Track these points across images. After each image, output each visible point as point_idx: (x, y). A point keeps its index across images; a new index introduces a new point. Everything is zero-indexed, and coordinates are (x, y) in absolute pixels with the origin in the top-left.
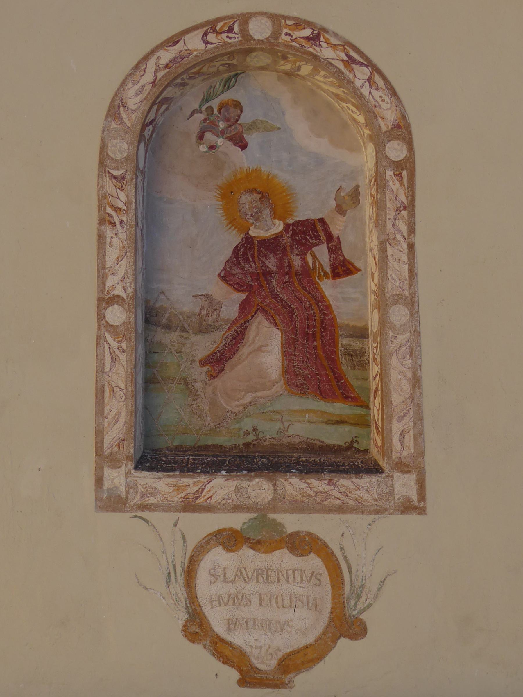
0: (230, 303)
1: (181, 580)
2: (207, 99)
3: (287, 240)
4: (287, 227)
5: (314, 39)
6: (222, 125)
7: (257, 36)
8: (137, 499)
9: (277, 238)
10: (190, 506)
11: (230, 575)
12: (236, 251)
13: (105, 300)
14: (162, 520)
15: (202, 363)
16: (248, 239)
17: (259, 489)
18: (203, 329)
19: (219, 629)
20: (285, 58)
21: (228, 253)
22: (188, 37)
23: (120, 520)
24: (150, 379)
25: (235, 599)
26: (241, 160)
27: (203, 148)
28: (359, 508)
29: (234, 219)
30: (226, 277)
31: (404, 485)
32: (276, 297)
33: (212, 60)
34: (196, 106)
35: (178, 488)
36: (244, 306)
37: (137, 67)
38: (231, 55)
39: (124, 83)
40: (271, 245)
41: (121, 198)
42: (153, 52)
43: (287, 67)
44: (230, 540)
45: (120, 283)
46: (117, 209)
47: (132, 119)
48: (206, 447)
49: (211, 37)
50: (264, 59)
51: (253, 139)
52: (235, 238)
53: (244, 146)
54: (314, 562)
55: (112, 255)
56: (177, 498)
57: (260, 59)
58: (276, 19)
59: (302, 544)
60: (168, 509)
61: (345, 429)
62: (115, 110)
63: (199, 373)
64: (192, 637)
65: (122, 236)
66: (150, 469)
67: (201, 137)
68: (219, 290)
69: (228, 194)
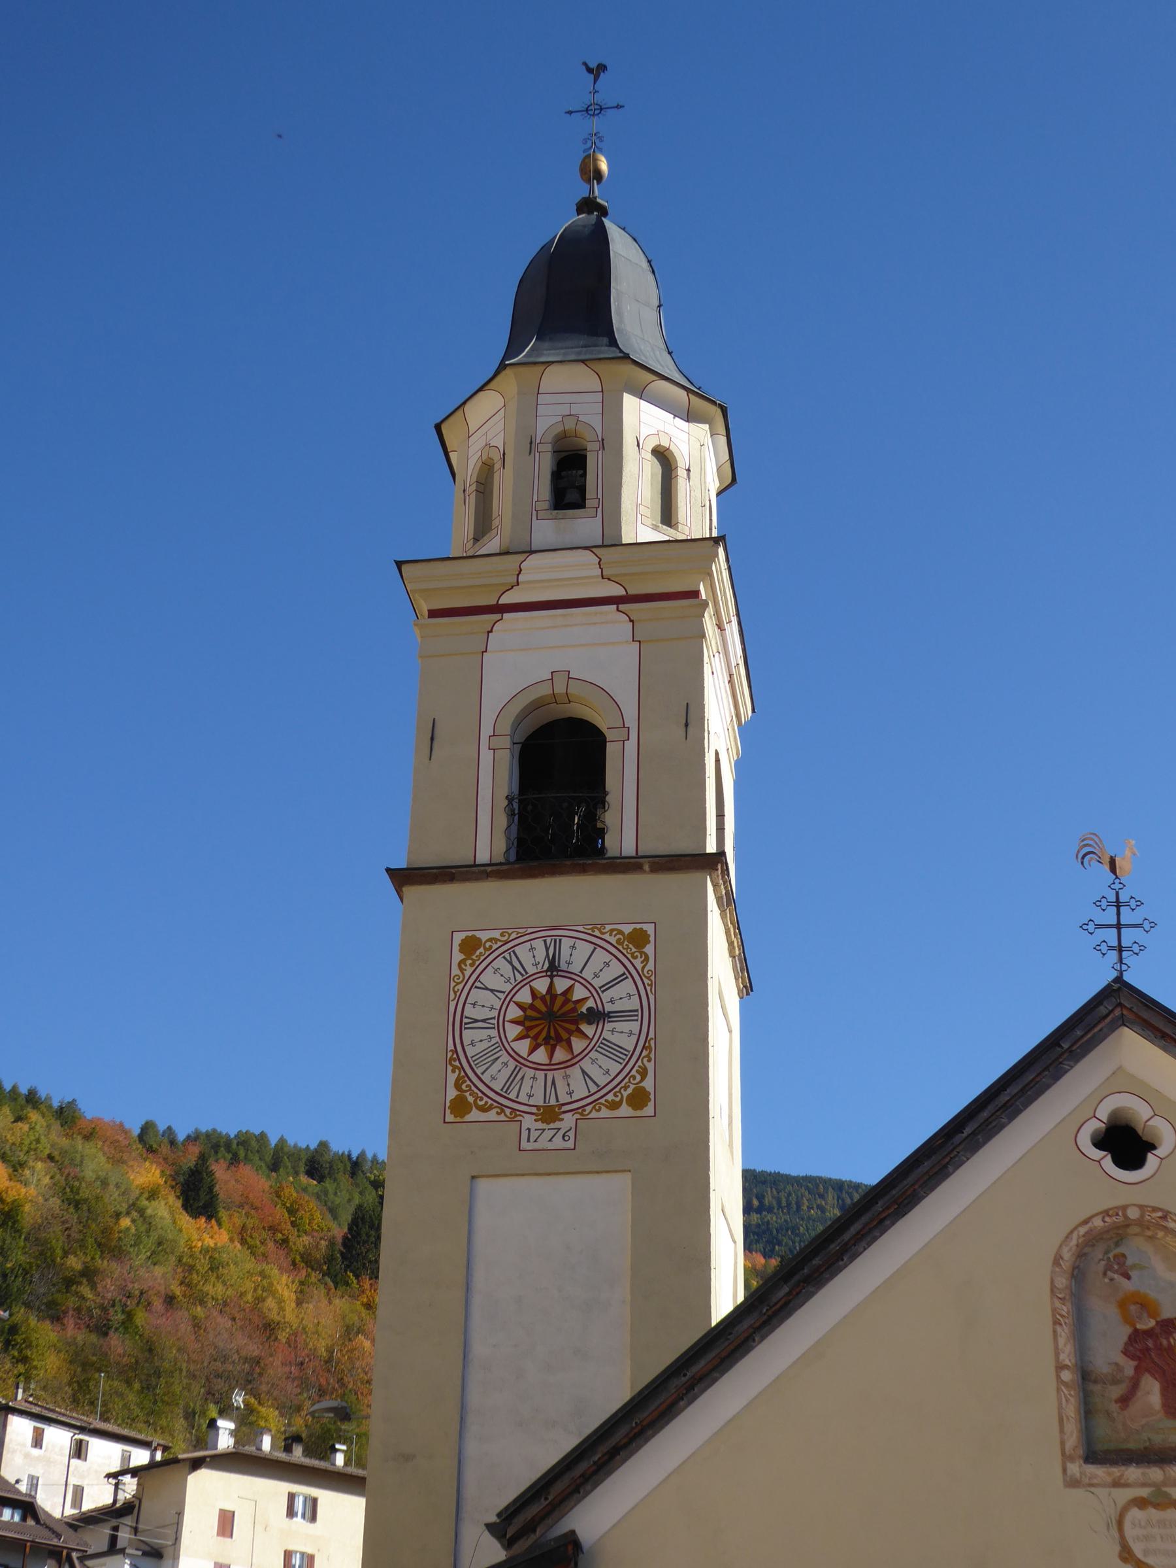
0: (1129, 1367)
1: (1115, 1527)
2: (1106, 1252)
3: (1158, 1330)
4: (1157, 1323)
5: (1164, 1218)
6: (1116, 1267)
7: (1132, 1217)
8: (1086, 1481)
9: (1152, 1329)
10: (1117, 1484)
11: (1143, 1524)
12: (1130, 1338)
13: (1060, 1367)
14: (1102, 1492)
15: (1116, 1402)
16: (1136, 1331)
17: (1155, 1473)
18: (1115, 1382)
19: (1140, 1555)
20: (1148, 1229)
21: (1125, 1338)
22: (1094, 1220)
23: (1079, 1493)
24: (1088, 1412)
25: (1147, 1538)
27: (1107, 1280)
29: (1127, 1319)
30: (1125, 1352)
32: (1154, 1362)
33: (1108, 1231)
34: (1101, 1257)
35: (1109, 1474)
36: (1137, 1368)
37: (1067, 1237)
38: (1118, 1228)
39: (1061, 1246)
40: (1149, 1333)
41: (1064, 1310)
42: (1075, 1228)
43: (1149, 1233)
44: (1141, 1503)
45: (1067, 1358)
46: (1062, 1316)
47: (1066, 1264)
48: (1122, 1450)
49: (1107, 1219)
50: (1136, 1229)
51: (1132, 1274)
52: (1126, 1331)
53: (1129, 1278)
55: (1061, 1341)
56: (1109, 1479)
57: (1135, 1229)
58: (1141, 1207)
60: (1103, 1485)
62: (1057, 1261)
63: (1114, 1407)
64: (1124, 1560)
65: (1066, 1330)
66: (1093, 1463)
67: (1105, 1274)
68: (1122, 1360)
69: (1123, 1305)
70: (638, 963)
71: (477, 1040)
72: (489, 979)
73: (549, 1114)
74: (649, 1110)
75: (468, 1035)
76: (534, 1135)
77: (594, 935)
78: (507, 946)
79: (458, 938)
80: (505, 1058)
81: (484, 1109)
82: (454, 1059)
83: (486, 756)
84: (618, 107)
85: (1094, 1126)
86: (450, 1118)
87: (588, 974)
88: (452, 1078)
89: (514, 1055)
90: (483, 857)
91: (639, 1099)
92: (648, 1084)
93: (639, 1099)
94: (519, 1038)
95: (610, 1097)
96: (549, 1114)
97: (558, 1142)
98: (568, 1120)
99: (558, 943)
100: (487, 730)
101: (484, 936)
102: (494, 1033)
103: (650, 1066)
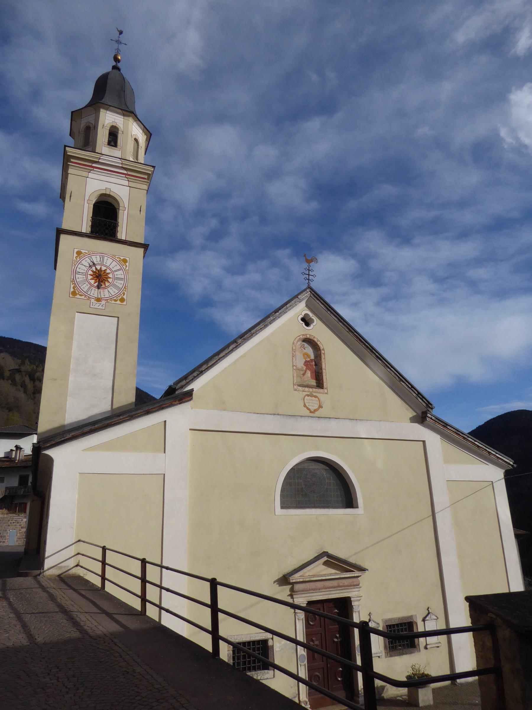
0: (305, 368)
10: (303, 391)
25: (309, 403)
26: (305, 351)
28: (321, 393)
29: (304, 358)
31: (326, 391)
40: (308, 361)
44: (308, 395)
54: (317, 399)
59: (316, 397)
61: (265, 677)
68: (303, 366)
69: (304, 355)
70: (124, 267)
71: (80, 278)
72: (84, 262)
73: (98, 300)
74: (125, 303)
75: (77, 276)
76: (94, 304)
77: (113, 257)
78: (90, 254)
79: (76, 250)
80: (87, 283)
81: (81, 295)
82: (73, 281)
83: (86, 205)
84: (125, 44)
85: (301, 316)
86: (71, 296)
87: (111, 267)
88: (72, 286)
89: (90, 284)
90: (84, 231)
91: (122, 300)
92: (125, 297)
93: (122, 300)
94: (91, 279)
95: (115, 298)
96: (98, 300)
97: (100, 307)
98: (103, 302)
99: (103, 257)
100: (87, 198)
101: (83, 251)
102: (85, 277)
103: (126, 293)
